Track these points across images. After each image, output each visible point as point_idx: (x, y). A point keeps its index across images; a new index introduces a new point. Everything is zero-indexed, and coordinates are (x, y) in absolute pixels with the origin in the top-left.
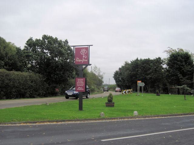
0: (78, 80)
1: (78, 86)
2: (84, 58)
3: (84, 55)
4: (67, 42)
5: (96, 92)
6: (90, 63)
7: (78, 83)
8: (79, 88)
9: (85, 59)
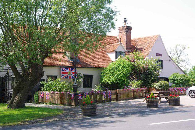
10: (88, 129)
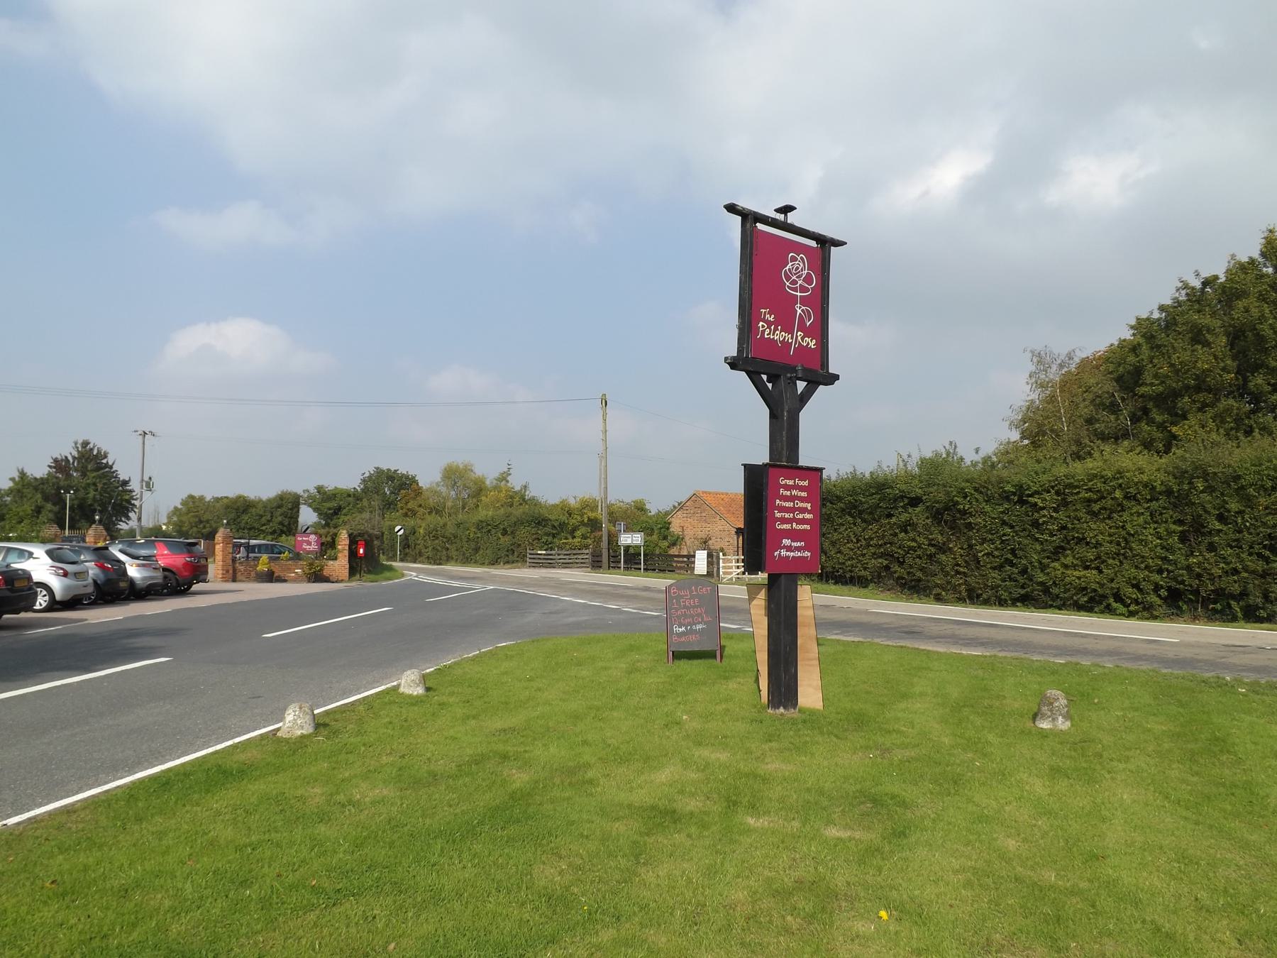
2: (802, 327)
3: (804, 301)
8: (786, 542)
9: (808, 332)
10: (39, 469)
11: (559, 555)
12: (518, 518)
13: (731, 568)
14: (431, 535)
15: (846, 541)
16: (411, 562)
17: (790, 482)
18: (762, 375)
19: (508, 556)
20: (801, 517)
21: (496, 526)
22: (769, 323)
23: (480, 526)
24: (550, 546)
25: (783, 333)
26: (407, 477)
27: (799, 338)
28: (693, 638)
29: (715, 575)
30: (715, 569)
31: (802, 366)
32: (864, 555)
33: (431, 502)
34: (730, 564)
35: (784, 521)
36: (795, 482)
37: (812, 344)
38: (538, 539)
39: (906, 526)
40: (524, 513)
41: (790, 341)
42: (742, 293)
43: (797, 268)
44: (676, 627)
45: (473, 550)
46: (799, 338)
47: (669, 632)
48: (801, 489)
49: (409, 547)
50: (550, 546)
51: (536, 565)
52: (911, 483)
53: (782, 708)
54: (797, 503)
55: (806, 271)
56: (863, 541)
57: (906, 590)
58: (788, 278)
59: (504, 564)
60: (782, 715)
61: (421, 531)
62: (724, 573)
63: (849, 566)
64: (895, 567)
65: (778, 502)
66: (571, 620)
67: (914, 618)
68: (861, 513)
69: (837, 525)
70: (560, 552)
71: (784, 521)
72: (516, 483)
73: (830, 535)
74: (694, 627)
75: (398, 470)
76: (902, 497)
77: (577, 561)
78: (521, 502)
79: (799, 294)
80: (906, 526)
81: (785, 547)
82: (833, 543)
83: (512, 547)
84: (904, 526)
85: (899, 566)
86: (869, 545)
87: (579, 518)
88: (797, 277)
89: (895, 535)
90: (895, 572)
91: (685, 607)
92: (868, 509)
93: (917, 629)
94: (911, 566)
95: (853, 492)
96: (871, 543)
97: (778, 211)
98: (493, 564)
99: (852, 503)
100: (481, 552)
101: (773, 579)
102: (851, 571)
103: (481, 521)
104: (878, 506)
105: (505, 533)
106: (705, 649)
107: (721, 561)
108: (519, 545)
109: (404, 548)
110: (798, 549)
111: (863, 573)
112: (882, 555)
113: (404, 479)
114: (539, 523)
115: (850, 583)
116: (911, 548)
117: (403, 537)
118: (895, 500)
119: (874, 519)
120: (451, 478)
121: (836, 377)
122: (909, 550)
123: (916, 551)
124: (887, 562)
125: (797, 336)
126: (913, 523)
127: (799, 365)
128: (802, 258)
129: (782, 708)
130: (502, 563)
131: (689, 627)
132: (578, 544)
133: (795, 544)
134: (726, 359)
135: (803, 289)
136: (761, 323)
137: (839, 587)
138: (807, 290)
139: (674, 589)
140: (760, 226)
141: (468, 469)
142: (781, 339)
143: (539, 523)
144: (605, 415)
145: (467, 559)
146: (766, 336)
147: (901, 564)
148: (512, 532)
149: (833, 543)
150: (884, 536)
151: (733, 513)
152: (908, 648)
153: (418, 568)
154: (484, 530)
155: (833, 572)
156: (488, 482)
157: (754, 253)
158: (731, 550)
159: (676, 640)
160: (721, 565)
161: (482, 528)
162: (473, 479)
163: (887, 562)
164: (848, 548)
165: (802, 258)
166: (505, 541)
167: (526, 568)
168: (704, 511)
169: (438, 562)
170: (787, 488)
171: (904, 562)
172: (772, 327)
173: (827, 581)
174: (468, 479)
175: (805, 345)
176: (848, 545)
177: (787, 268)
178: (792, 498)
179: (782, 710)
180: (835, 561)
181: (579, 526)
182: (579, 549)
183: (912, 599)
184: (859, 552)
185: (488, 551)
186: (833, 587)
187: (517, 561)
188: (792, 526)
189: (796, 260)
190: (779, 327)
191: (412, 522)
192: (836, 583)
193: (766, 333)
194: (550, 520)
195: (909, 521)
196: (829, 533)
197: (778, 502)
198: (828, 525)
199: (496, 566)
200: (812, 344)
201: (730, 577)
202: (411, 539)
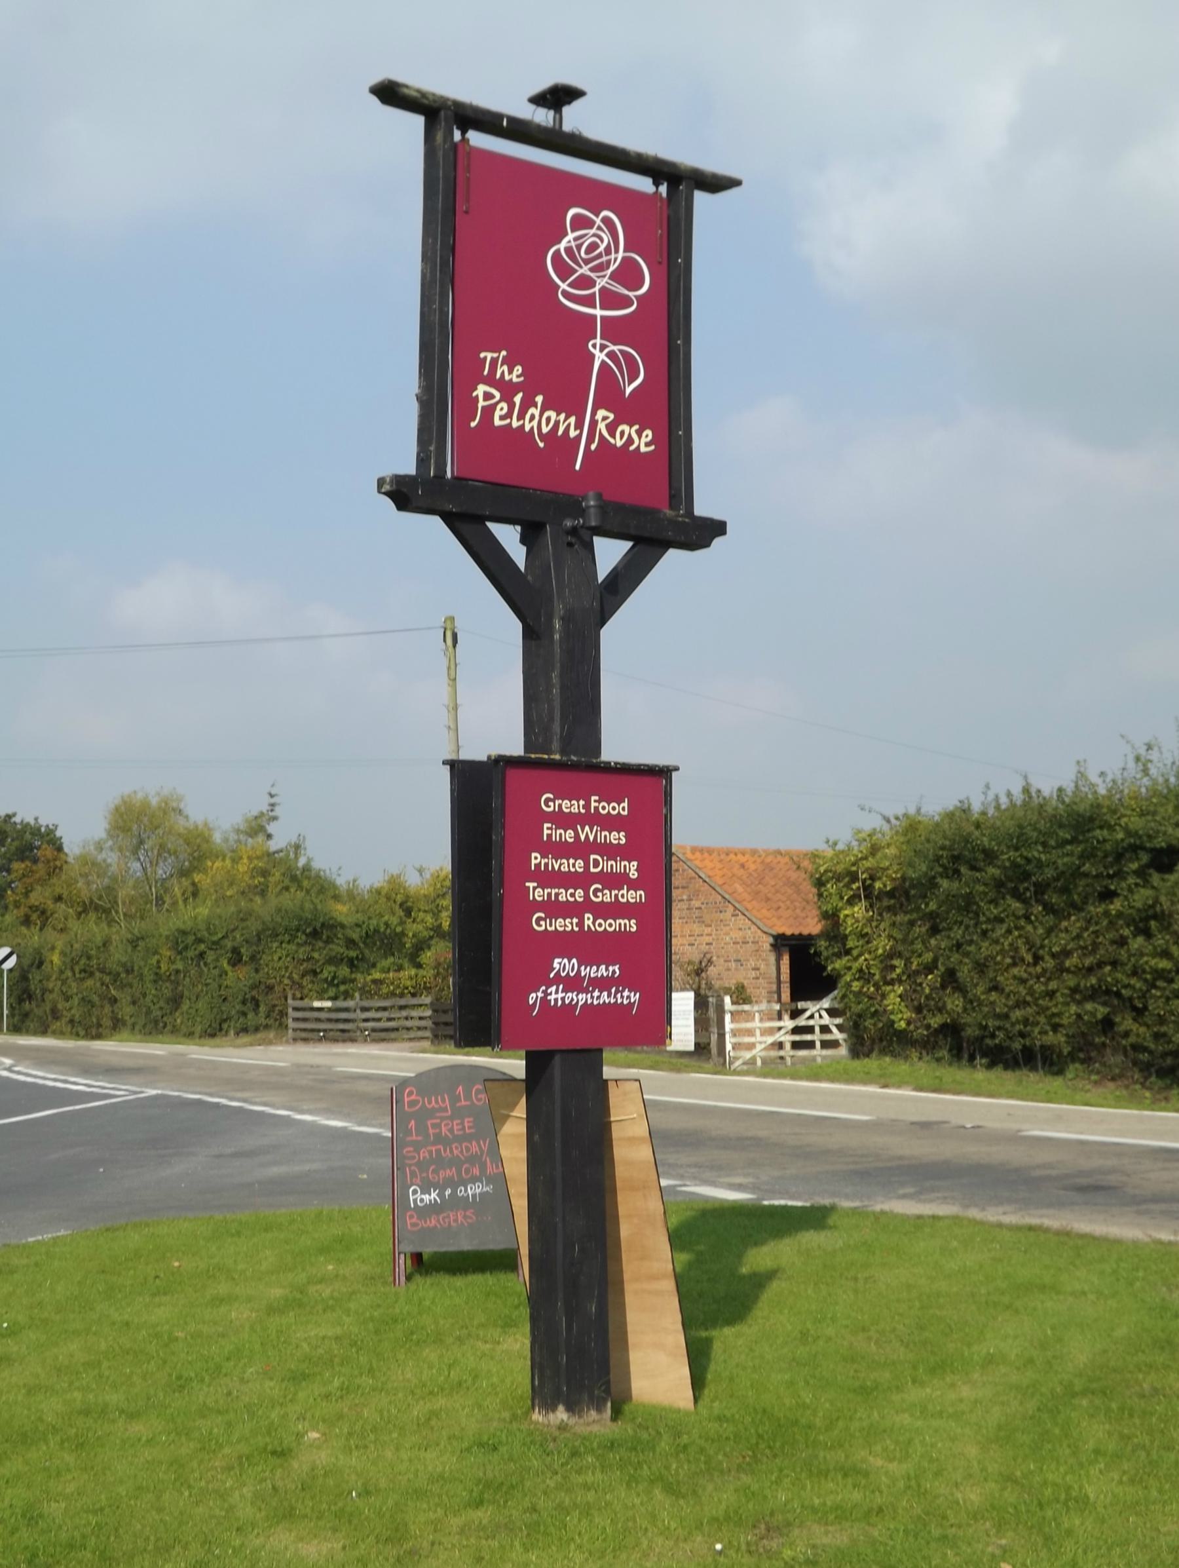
0: (549, 803)
1: (540, 924)
2: (609, 395)
3: (613, 330)
4: (399, 480)
5: (709, 1066)
6: (701, 509)
7: (548, 879)
8: (562, 965)
9: (625, 411)
11: (364, 1009)
12: (264, 923)
13: (750, 1032)
14: (77, 969)
15: (1008, 960)
16: (35, 1033)
17: (573, 807)
18: (495, 528)
19: (244, 1014)
20: (607, 899)
21: (214, 943)
22: (508, 391)
23: (182, 941)
24: (342, 988)
25: (552, 414)
26: (36, 831)
27: (602, 426)
28: (457, 1218)
29: (714, 1050)
30: (714, 1038)
31: (599, 497)
32: (1051, 994)
33: (84, 890)
34: (749, 1025)
35: (554, 909)
36: (587, 806)
37: (645, 442)
38: (315, 973)
39: (1147, 919)
40: (279, 910)
41: (573, 433)
42: (426, 309)
43: (593, 247)
44: (415, 1192)
45: (168, 1001)
46: (602, 426)
47: (398, 1203)
48: (610, 823)
49: (30, 997)
50: (342, 988)
51: (308, 1036)
52: (1154, 813)
53: (561, 1408)
54: (596, 864)
55: (621, 254)
56: (1047, 958)
57: (1153, 1079)
58: (564, 271)
59: (237, 1034)
60: (562, 1427)
61: (56, 958)
62: (736, 1047)
63: (1018, 1022)
64: (1126, 1022)
65: (536, 858)
66: (275, 1171)
67: (1119, 1150)
68: (1041, 889)
69: (989, 921)
70: (366, 1004)
71: (554, 909)
72: (281, 837)
73: (972, 948)
74: (461, 1192)
75: (14, 815)
76: (1135, 849)
77: (409, 1023)
78: (287, 882)
79: (598, 312)
80: (1147, 919)
81: (558, 979)
82: (981, 967)
83: (254, 993)
84: (1141, 920)
85: (1135, 1020)
86: (1061, 970)
87: (429, 919)
88: (592, 270)
89: (1122, 942)
90: (1126, 1034)
91: (439, 1139)
92: (1057, 879)
93: (1112, 1179)
94: (1162, 1020)
95: (1019, 840)
96: (1067, 963)
97: (539, 100)
98: (213, 1036)
99: (1019, 866)
100: (185, 1006)
101: (537, 1062)
102: (1022, 1035)
103: (184, 933)
104: (1077, 874)
105: (236, 959)
106: (491, 1247)
107: (728, 1018)
108: (270, 988)
109: (21, 1001)
110: (602, 984)
111: (1050, 1038)
112: (1094, 994)
113: (28, 836)
114: (315, 934)
115: (1025, 1065)
116: (1159, 974)
117: (16, 974)
118: (1119, 857)
119: (1073, 905)
120: (130, 830)
121: (717, 528)
122: (1155, 979)
123: (1171, 981)
124: (1107, 1010)
125: (594, 423)
126: (1163, 912)
127: (591, 494)
128: (607, 222)
129: (561, 1408)
130: (232, 1032)
131: (448, 1192)
132: (409, 983)
133: (592, 972)
134: (381, 482)
135: (610, 299)
136: (481, 389)
137: (999, 1076)
138: (625, 302)
139: (411, 1093)
140: (478, 139)
141: (170, 808)
142: (545, 430)
143: (315, 934)
144: (452, 667)
145: (156, 1022)
146: (497, 422)
147: (1139, 1013)
148: (253, 958)
149: (981, 967)
150: (1095, 946)
151: (768, 899)
152: (1047, 1230)
153: (37, 1049)
154: (191, 953)
155: (983, 1037)
156: (217, 838)
157: (461, 206)
158: (761, 988)
159: (415, 1225)
160: (729, 1025)
161: (186, 948)
162: (181, 830)
163: (1107, 1010)
164: (1015, 977)
165: (607, 222)
166: (239, 978)
167: (287, 1042)
168: (697, 893)
169: (94, 1031)
170: (563, 820)
171: (1145, 1008)
172: (518, 399)
173: (972, 1058)
174: (170, 832)
175: (619, 443)
176: (1015, 971)
177: (562, 246)
178: (580, 850)
179: (561, 1414)
180: (986, 1009)
181: (431, 938)
182: (414, 995)
183: (1167, 1099)
184: (1038, 988)
185: (200, 1005)
186: (980, 1075)
187: (267, 1027)
188: (581, 924)
189: (589, 224)
190: (539, 399)
191: (33, 938)
192: (991, 1066)
193: (497, 414)
194: (343, 926)
195: (1151, 907)
196: (971, 942)
197: (536, 858)
198: (966, 921)
199: (217, 1040)
200: (645, 442)
201: (748, 1055)
202: (35, 977)
